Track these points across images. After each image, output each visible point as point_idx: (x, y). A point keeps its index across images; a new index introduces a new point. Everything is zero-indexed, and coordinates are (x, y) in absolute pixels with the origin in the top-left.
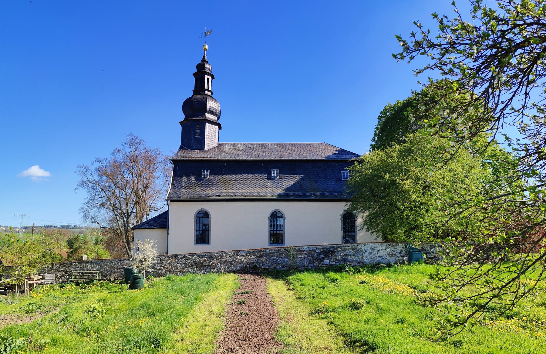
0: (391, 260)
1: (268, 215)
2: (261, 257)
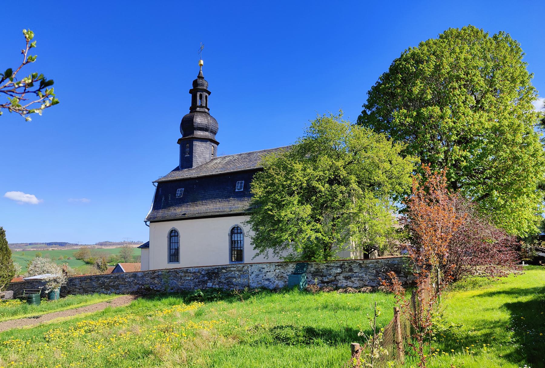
0: (280, 283)
1: (228, 231)
2: (154, 278)
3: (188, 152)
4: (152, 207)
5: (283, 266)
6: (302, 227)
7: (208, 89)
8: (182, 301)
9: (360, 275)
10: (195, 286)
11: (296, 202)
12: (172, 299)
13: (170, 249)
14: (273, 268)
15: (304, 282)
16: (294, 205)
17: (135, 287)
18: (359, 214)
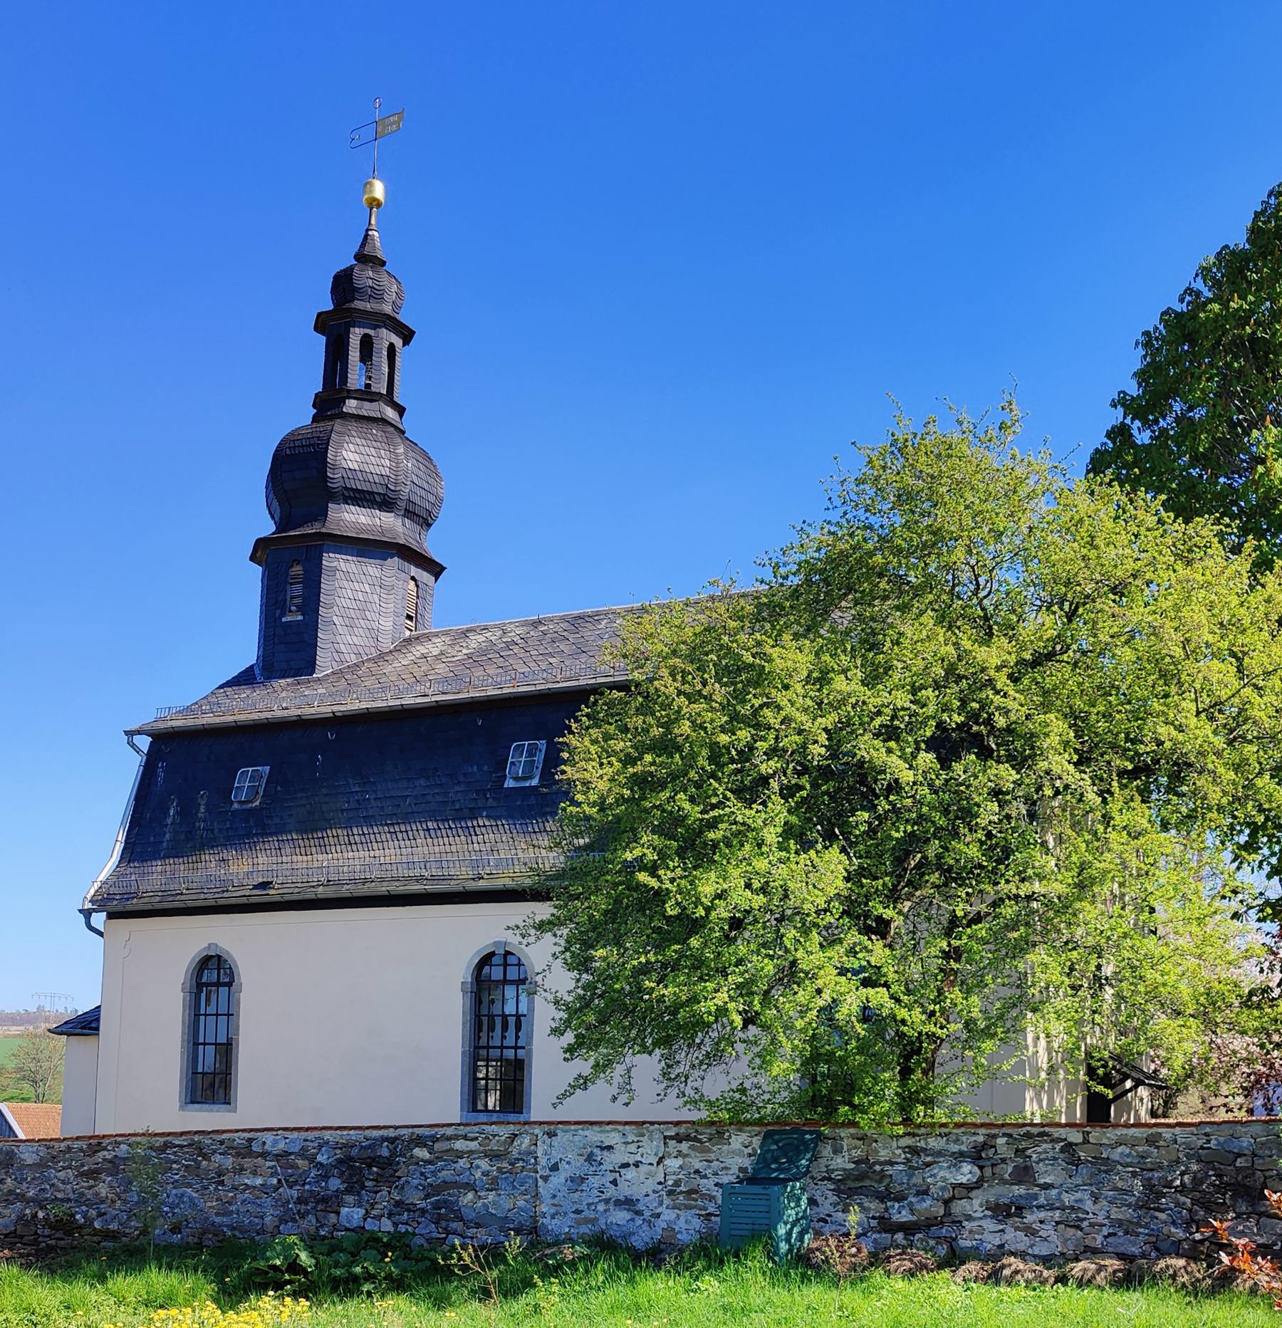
0: (681, 1223)
1: (462, 971)
2: (93, 1174)
3: (296, 601)
4: (119, 848)
5: (700, 1141)
6: (800, 954)
7: (398, 317)
8: (211, 1288)
9: (1067, 1199)
10: (283, 1221)
11: (771, 835)
12: (158, 1279)
13: (194, 1042)
14: (651, 1147)
15: (794, 1225)
16: (764, 849)
17: (7, 1212)
18: (1077, 905)
